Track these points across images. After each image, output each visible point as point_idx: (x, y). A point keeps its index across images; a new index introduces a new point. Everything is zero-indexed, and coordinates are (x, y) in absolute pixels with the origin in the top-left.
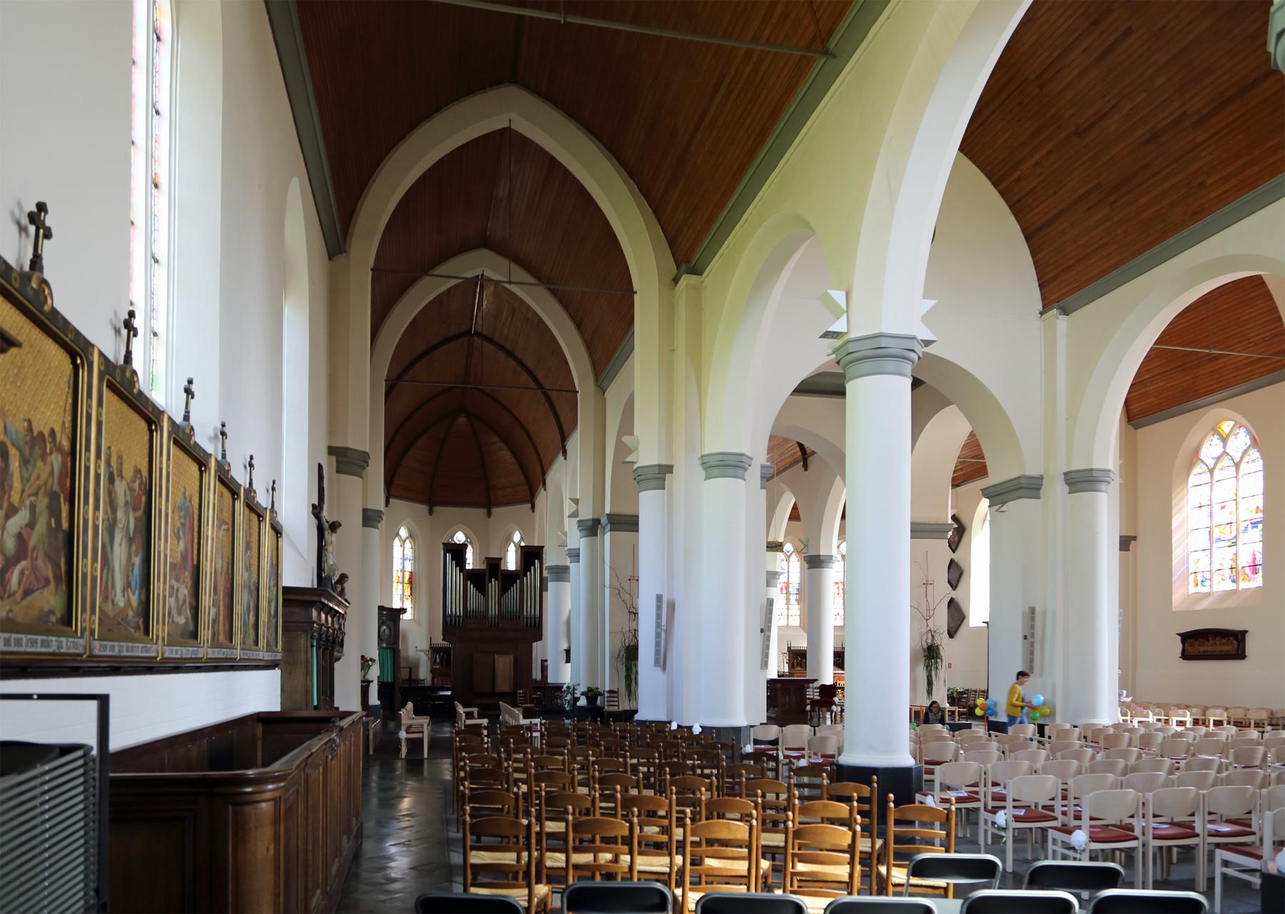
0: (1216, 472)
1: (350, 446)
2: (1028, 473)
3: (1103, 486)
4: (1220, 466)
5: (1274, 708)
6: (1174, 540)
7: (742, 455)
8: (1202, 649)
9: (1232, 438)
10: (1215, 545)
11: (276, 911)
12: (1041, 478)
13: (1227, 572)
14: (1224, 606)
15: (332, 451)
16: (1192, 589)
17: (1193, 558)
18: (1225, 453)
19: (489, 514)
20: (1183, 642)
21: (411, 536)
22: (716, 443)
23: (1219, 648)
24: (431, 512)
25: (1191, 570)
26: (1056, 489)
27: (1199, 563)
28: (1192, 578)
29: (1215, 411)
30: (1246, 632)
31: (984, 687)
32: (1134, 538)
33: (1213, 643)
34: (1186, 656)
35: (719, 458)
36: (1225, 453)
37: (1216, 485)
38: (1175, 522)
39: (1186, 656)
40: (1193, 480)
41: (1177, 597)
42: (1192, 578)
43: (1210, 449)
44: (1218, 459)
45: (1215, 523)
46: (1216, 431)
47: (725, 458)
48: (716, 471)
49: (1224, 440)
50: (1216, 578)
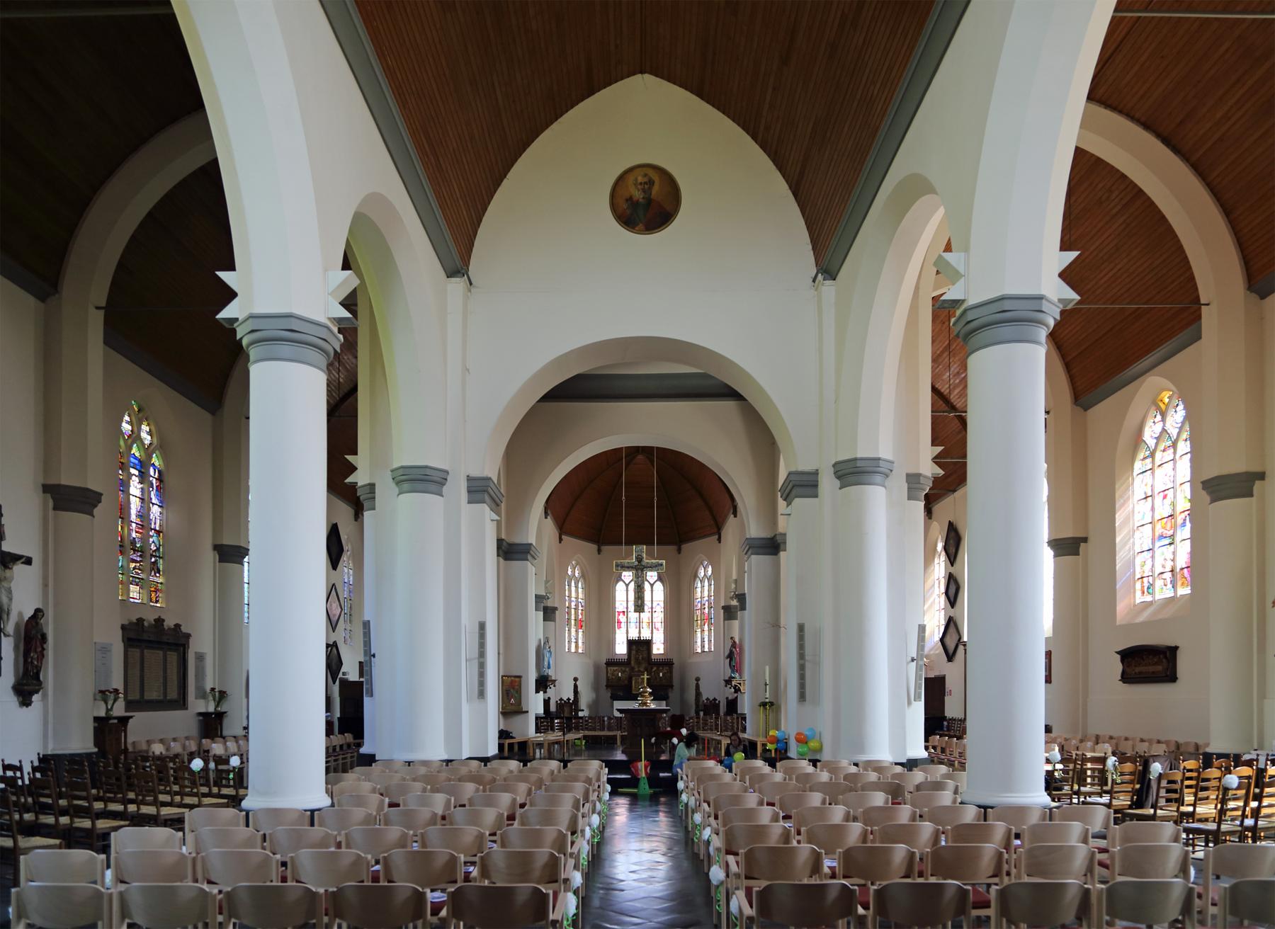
0: (1158, 455)
1: (63, 482)
2: (800, 468)
3: (878, 478)
4: (1161, 447)
5: (1181, 741)
6: (1118, 540)
7: (426, 467)
8: (1137, 670)
9: (1171, 411)
10: (1158, 544)
11: (875, 927)
12: (816, 473)
13: (1168, 576)
14: (1160, 617)
15: (47, 488)
16: (1139, 598)
17: (1138, 560)
18: (1164, 430)
19: (679, 551)
20: (1122, 661)
21: (583, 575)
22: (406, 455)
23: (1151, 669)
24: (599, 551)
25: (1138, 576)
26: (827, 482)
27: (1142, 565)
28: (1138, 585)
29: (1152, 381)
30: (1176, 648)
31: (961, 716)
32: (1085, 540)
33: (1149, 663)
34: (1126, 678)
35: (401, 472)
36: (1164, 430)
37: (1157, 471)
38: (1119, 517)
39: (1126, 678)
40: (1138, 466)
41: (1122, 607)
42: (1138, 585)
43: (1151, 432)
44: (1158, 439)
45: (1157, 517)
46: (1155, 403)
47: (407, 471)
48: (406, 486)
49: (1164, 415)
50: (1159, 583)
